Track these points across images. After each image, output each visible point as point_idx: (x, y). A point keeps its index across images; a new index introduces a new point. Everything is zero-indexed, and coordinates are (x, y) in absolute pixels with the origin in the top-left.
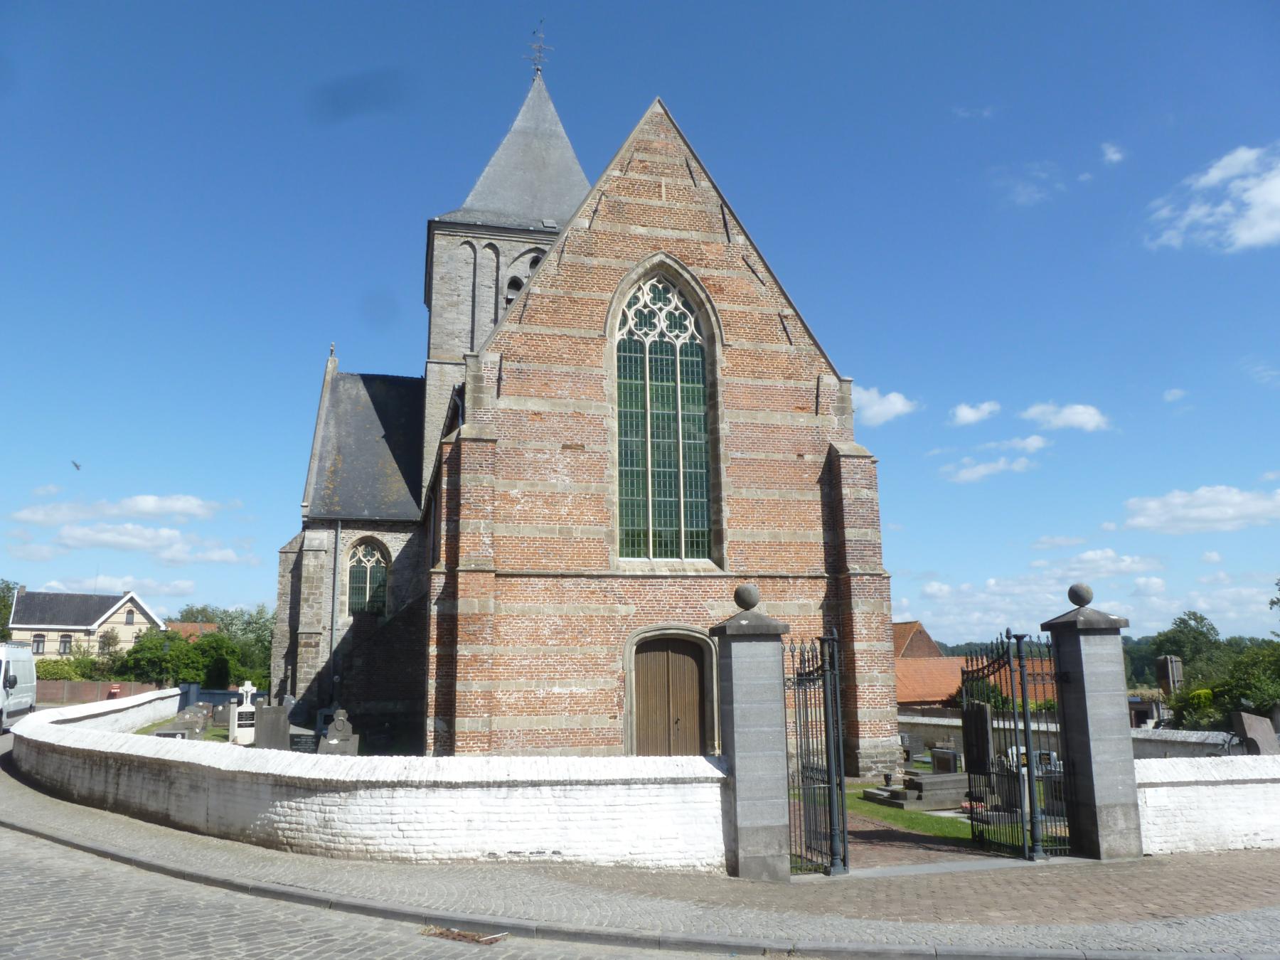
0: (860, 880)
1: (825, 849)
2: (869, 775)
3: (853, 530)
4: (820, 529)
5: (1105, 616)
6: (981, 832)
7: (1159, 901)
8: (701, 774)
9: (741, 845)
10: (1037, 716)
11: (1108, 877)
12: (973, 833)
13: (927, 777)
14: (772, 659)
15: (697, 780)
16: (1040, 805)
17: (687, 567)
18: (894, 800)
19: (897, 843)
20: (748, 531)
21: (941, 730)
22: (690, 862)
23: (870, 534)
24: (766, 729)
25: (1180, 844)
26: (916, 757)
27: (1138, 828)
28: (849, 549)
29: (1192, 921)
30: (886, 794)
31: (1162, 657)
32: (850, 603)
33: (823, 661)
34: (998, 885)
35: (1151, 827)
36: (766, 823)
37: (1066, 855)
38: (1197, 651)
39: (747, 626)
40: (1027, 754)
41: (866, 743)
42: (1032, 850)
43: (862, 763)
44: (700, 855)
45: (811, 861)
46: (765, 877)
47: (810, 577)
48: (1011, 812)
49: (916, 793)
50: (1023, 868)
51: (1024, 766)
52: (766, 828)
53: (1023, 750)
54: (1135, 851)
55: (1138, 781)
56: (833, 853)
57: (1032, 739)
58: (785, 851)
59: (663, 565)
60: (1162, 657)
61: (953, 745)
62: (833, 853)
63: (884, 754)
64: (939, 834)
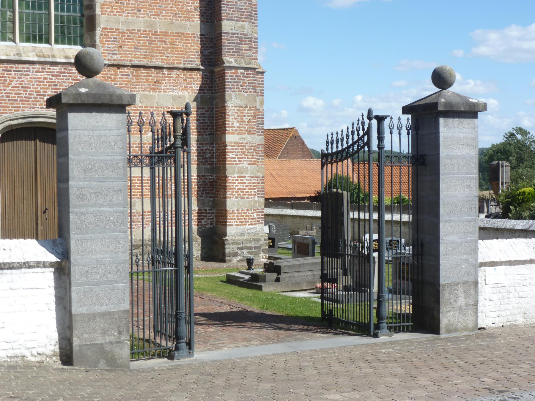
0: (204, 363)
1: (171, 332)
2: (235, 260)
3: (230, 23)
4: (197, 21)
5: (465, 99)
6: (331, 312)
7: (494, 374)
8: (31, 258)
9: (75, 333)
10: (390, 209)
11: (446, 350)
12: (323, 312)
13: (286, 260)
14: (115, 132)
15: (27, 265)
16: (388, 284)
17: (56, 53)
18: (254, 282)
19: (249, 324)
20: (123, 19)
21: (306, 221)
22: (18, 352)
23: (246, 27)
24: (106, 209)
25: (510, 318)
26: (281, 244)
27: (476, 304)
28: (225, 41)
29: (526, 395)
30: (247, 277)
31: (495, 163)
32: (224, 97)
33: (175, 137)
34: (342, 363)
35: (487, 303)
36: (104, 309)
37: (408, 331)
38: (520, 160)
39: (86, 94)
40: (379, 241)
41: (233, 230)
42: (377, 327)
43: (229, 249)
44: (29, 345)
45: (159, 345)
46: (102, 365)
47: (185, 69)
48: (360, 291)
49: (274, 276)
50: (368, 345)
51: (375, 251)
52: (104, 315)
53: (375, 236)
54: (471, 325)
55: (480, 260)
56: (177, 338)
57: (384, 227)
58: (125, 338)
59: (30, 50)
60: (495, 163)
61: (314, 233)
62: (177, 338)
63: (249, 241)
64: (292, 313)
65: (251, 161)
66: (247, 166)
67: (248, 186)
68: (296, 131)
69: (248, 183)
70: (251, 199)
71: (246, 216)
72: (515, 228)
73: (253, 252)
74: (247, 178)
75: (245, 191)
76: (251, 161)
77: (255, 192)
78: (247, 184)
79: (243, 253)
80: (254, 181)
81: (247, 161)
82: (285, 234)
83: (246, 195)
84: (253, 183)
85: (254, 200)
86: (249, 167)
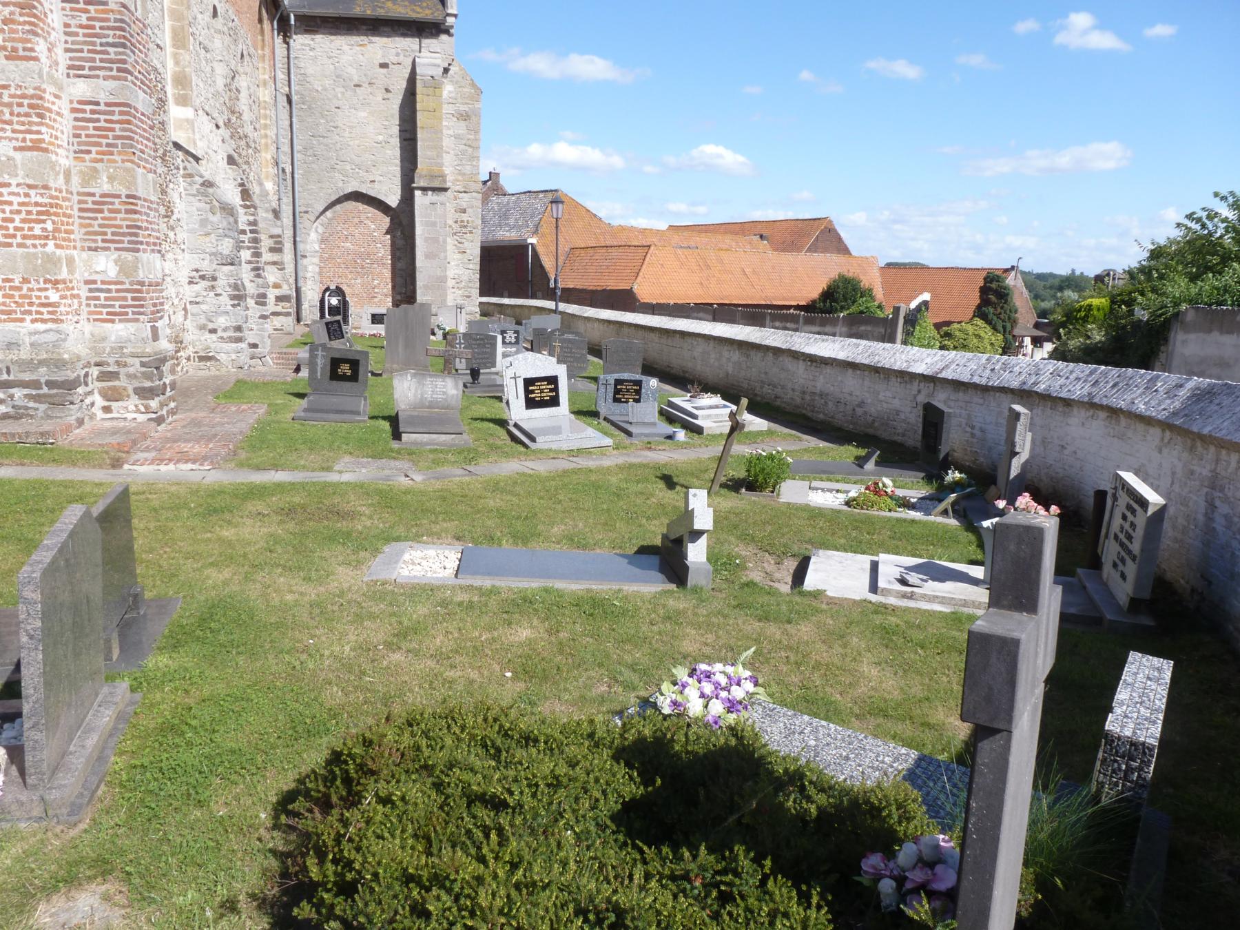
63: (29, 365)
65: (24, 140)
66: (11, 153)
67: (19, 212)
68: (830, 221)
69: (20, 204)
70: (32, 250)
71: (21, 297)
72: (911, 370)
73: (45, 395)
74: (14, 189)
75: (11, 226)
76: (24, 140)
77: (44, 230)
78: (15, 207)
79: (12, 397)
80: (39, 199)
81: (11, 139)
82: (486, 353)
83: (14, 236)
84: (37, 204)
85: (43, 253)
86: (18, 156)
